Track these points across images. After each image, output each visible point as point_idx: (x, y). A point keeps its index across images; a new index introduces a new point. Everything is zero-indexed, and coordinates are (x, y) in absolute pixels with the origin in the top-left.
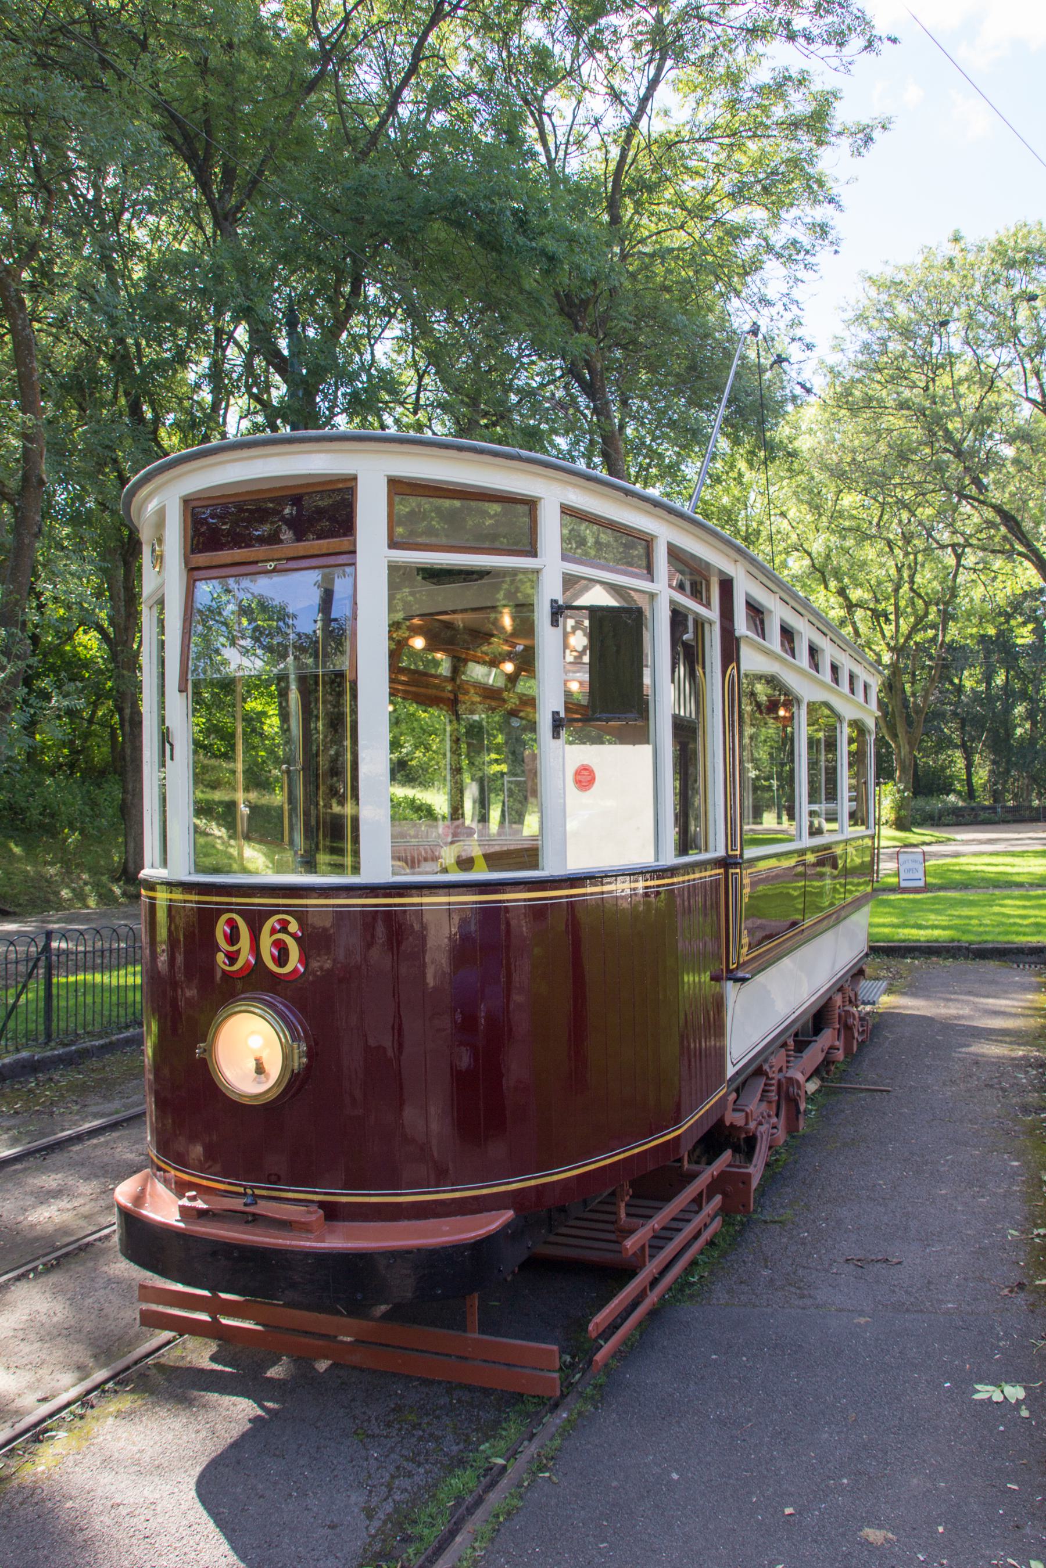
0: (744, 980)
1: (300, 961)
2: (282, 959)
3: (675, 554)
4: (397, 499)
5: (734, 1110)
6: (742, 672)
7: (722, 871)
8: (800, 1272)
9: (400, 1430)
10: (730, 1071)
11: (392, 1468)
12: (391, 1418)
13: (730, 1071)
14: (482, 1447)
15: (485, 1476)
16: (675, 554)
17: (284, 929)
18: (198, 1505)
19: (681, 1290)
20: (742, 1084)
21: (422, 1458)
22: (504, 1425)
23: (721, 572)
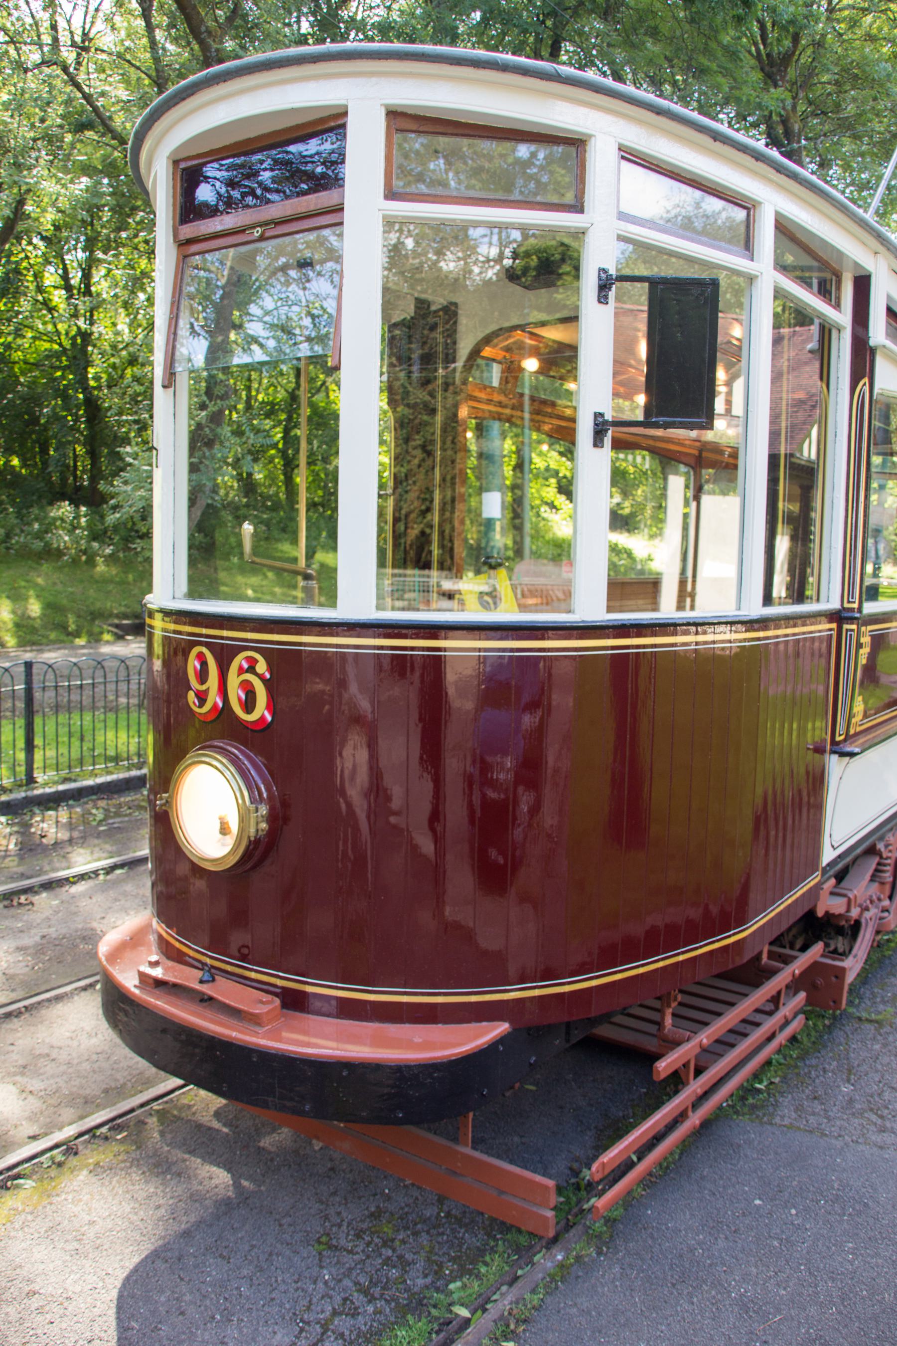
0: (852, 755)
1: (268, 708)
2: (249, 704)
4: (397, 137)
5: (832, 893)
6: (876, 391)
7: (834, 626)
8: (887, 1095)
9: (368, 1244)
10: (828, 855)
11: (338, 1299)
12: (364, 1226)
13: (828, 855)
14: (452, 1286)
15: (438, 1332)
17: (252, 670)
18: (112, 1312)
19: (743, 1098)
20: (842, 873)
21: (377, 1291)
22: (488, 1258)
23: (856, 265)
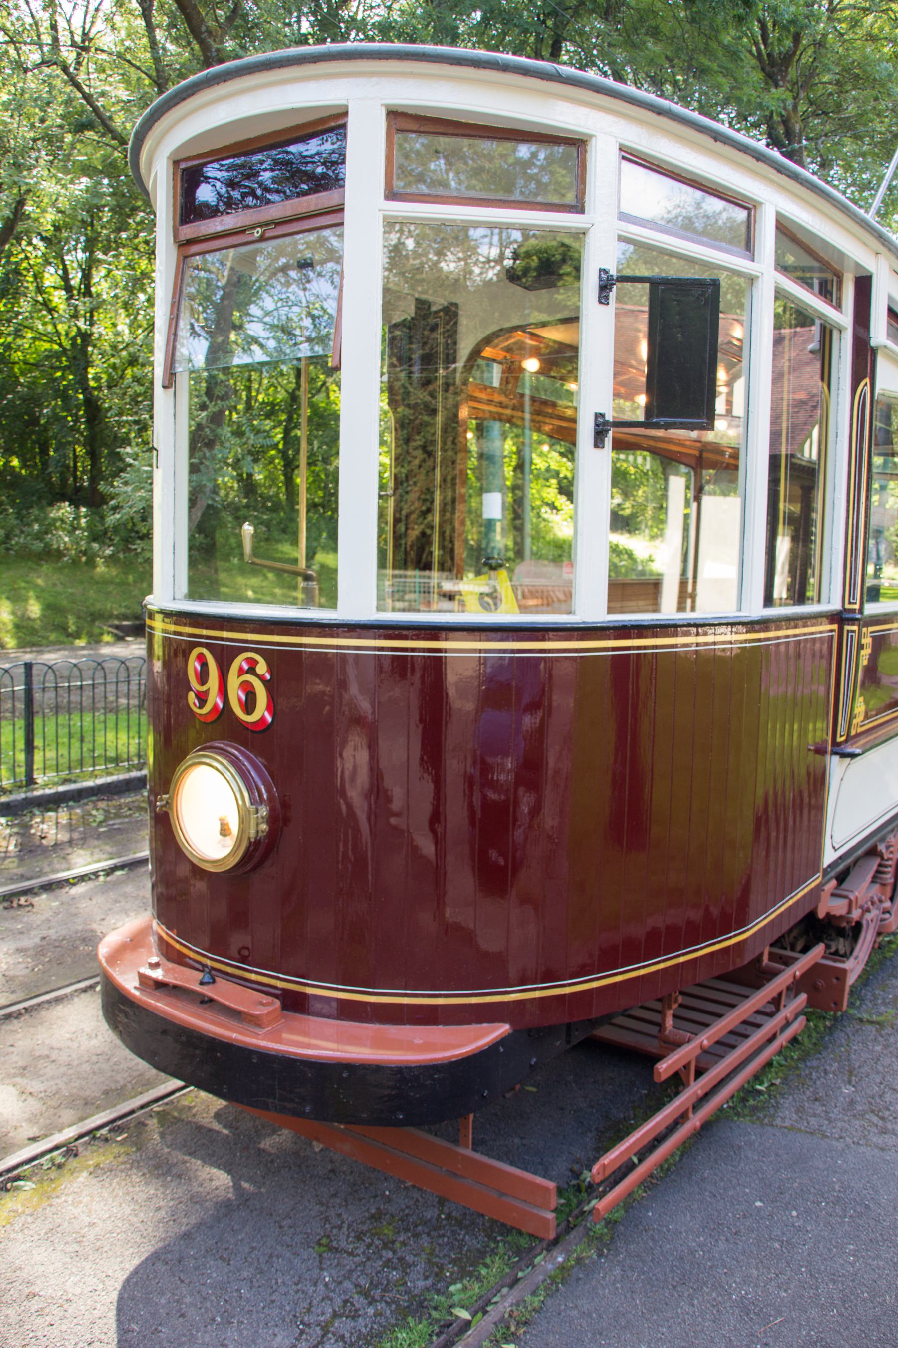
0: (853, 756)
1: (268, 709)
2: (249, 705)
3: (786, 230)
4: (398, 137)
5: (833, 895)
6: (877, 391)
7: (835, 626)
8: (888, 1097)
9: (369, 1246)
10: (829, 857)
11: (338, 1301)
12: (365, 1228)
13: (829, 857)
14: (452, 1288)
15: (438, 1334)
16: (786, 230)
17: (252, 671)
18: (112, 1314)
19: (744, 1100)
20: (843, 874)
21: (377, 1293)
22: (488, 1260)
23: (857, 265)
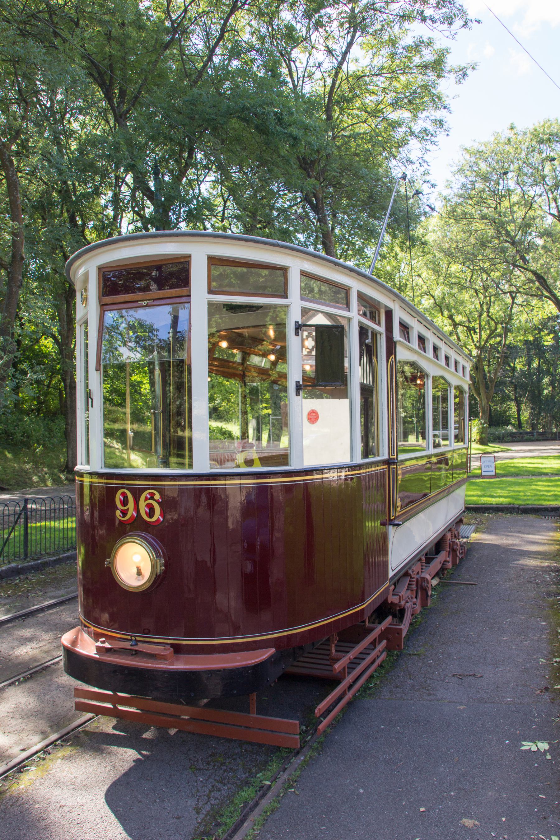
0: (398, 525)
1: (161, 515)
2: (151, 514)
3: (361, 297)
4: (213, 267)
5: (393, 595)
6: (397, 360)
7: (386, 466)
8: (429, 681)
9: (214, 766)
10: (391, 574)
11: (210, 787)
12: (209, 759)
13: (391, 574)
14: (258, 775)
15: (259, 791)
16: (361, 297)
17: (152, 498)
18: (106, 806)
19: (365, 691)
20: (397, 581)
21: (226, 781)
22: (270, 763)
23: (386, 306)
